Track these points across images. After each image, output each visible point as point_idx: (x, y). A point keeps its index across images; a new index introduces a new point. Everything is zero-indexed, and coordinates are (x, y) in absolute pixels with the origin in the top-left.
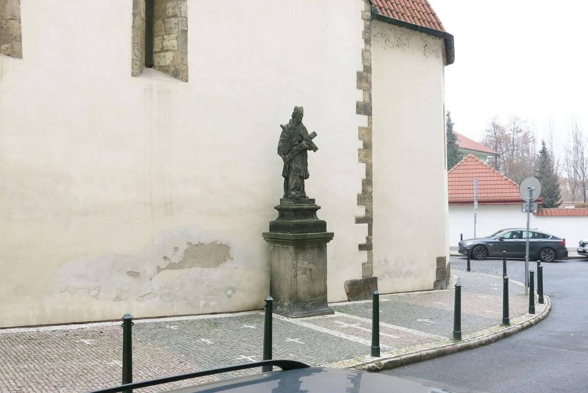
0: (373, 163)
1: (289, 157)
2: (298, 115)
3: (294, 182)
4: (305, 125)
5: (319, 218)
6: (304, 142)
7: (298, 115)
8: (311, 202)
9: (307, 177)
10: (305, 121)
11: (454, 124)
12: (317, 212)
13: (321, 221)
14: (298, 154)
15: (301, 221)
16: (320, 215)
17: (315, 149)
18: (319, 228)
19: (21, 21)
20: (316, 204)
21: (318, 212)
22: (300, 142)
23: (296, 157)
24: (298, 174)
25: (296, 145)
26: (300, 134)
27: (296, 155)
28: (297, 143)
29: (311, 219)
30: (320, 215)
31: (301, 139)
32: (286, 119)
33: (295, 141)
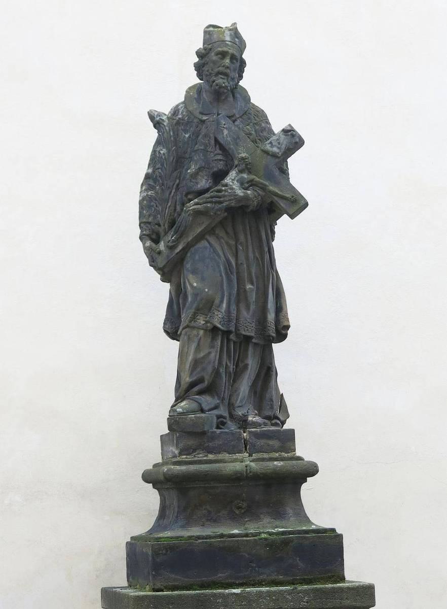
0: (241, 30)
1: (172, 248)
2: (221, 60)
3: (190, 358)
4: (256, 99)
5: (312, 518)
6: (232, 179)
7: (221, 60)
8: (275, 443)
9: (281, 335)
10: (252, 82)
11: (312, 470)
12: (304, 487)
13: (325, 531)
14: (210, 231)
15: (208, 531)
16: (319, 505)
17: (296, 205)
18: (301, 565)
19: (151, 124)
20: (298, 453)
21: (309, 491)
22: (219, 176)
23: (204, 243)
24: (201, 321)
25: (200, 193)
26: (216, 140)
27: (200, 237)
28: (203, 183)
29: (266, 520)
30: (319, 505)
31: (221, 166)
32: (173, 83)
33: (195, 175)
